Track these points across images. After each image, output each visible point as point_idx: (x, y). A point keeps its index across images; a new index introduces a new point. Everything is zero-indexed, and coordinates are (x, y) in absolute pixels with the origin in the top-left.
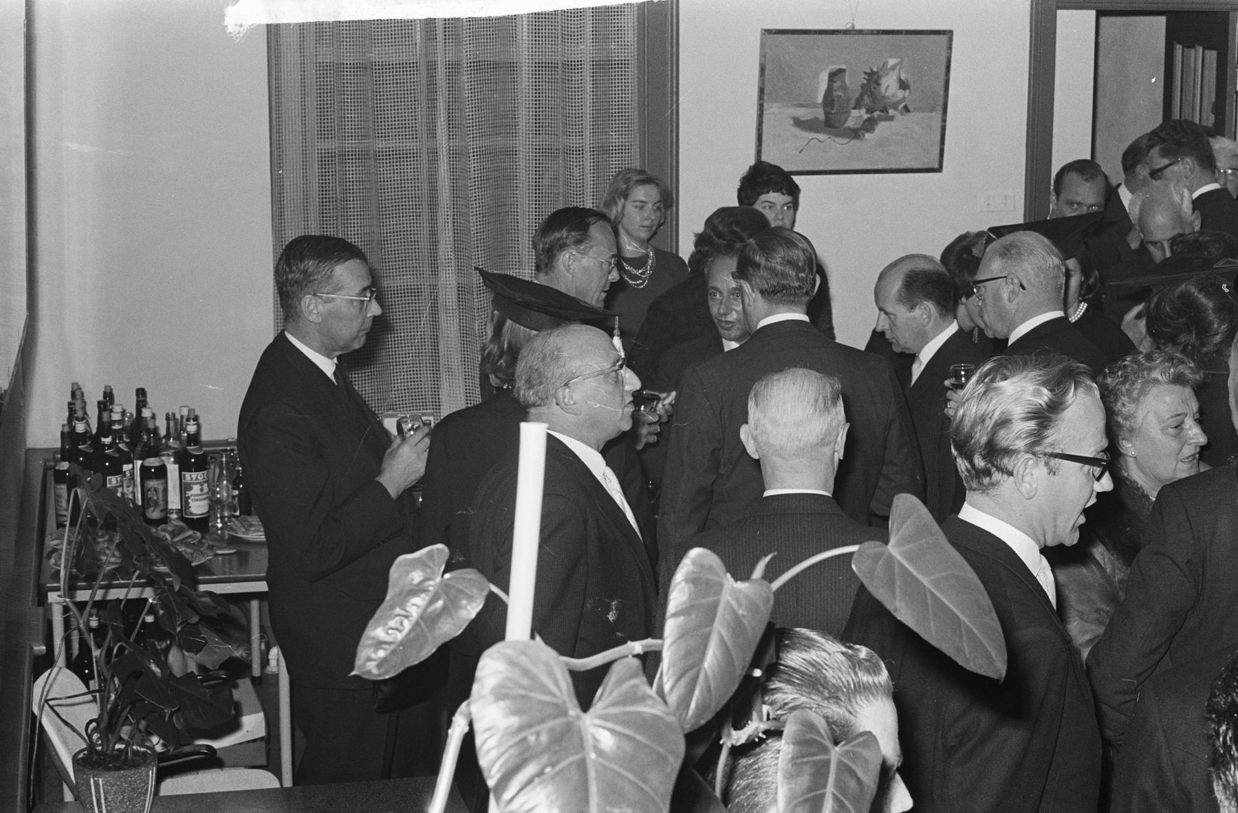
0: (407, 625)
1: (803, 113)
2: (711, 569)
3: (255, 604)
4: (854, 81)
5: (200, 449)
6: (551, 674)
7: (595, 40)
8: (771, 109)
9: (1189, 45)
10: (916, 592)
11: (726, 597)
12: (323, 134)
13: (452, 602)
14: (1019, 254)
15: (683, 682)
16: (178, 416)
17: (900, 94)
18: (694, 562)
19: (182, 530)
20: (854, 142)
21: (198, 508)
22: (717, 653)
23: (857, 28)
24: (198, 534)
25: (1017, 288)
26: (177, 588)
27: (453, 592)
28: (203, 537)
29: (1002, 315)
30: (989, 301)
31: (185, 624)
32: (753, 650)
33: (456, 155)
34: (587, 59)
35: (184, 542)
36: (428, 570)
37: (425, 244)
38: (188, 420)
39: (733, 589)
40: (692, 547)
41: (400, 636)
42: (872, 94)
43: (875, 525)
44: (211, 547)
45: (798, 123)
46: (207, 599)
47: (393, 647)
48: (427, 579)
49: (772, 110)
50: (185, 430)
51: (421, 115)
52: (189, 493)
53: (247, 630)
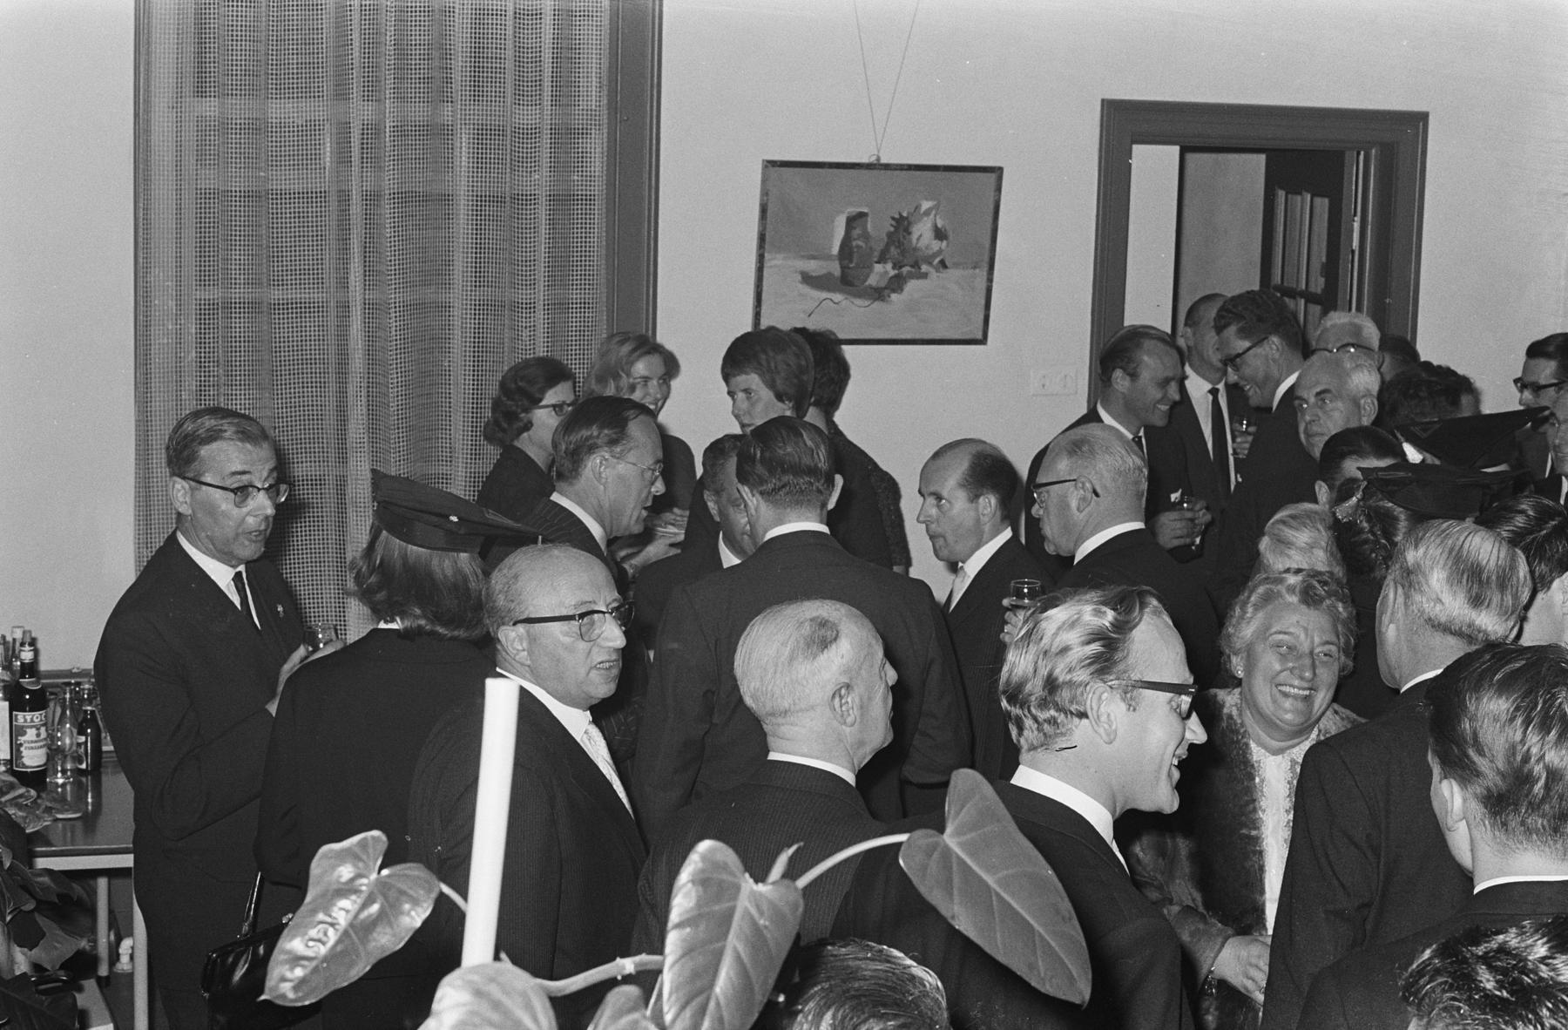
0: (333, 936)
1: (813, 267)
2: (724, 867)
3: (102, 883)
4: (878, 228)
5: (37, 683)
6: (529, 1007)
7: (553, 168)
8: (774, 261)
9: (1294, 190)
10: (979, 894)
11: (743, 903)
12: (203, 280)
13: (392, 906)
14: (1092, 452)
15: (688, 1013)
16: (9, 639)
17: (936, 245)
18: (704, 858)
19: (12, 787)
20: (877, 305)
21: (33, 758)
22: (732, 974)
23: (883, 161)
24: (33, 793)
25: (1089, 495)
26: (7, 865)
27: (392, 894)
28: (39, 797)
29: (1067, 527)
30: (1053, 510)
31: (18, 912)
32: (778, 970)
33: (371, 308)
34: (543, 193)
35: (14, 802)
36: (361, 865)
37: (330, 421)
38: (22, 644)
39: (753, 893)
40: (701, 839)
41: (323, 950)
42: (900, 245)
43: (924, 808)
44: (48, 810)
45: (807, 279)
46: (46, 879)
47: (314, 963)
48: (359, 876)
49: (774, 262)
50: (18, 658)
51: (329, 257)
52: (22, 739)
53: (92, 912)
